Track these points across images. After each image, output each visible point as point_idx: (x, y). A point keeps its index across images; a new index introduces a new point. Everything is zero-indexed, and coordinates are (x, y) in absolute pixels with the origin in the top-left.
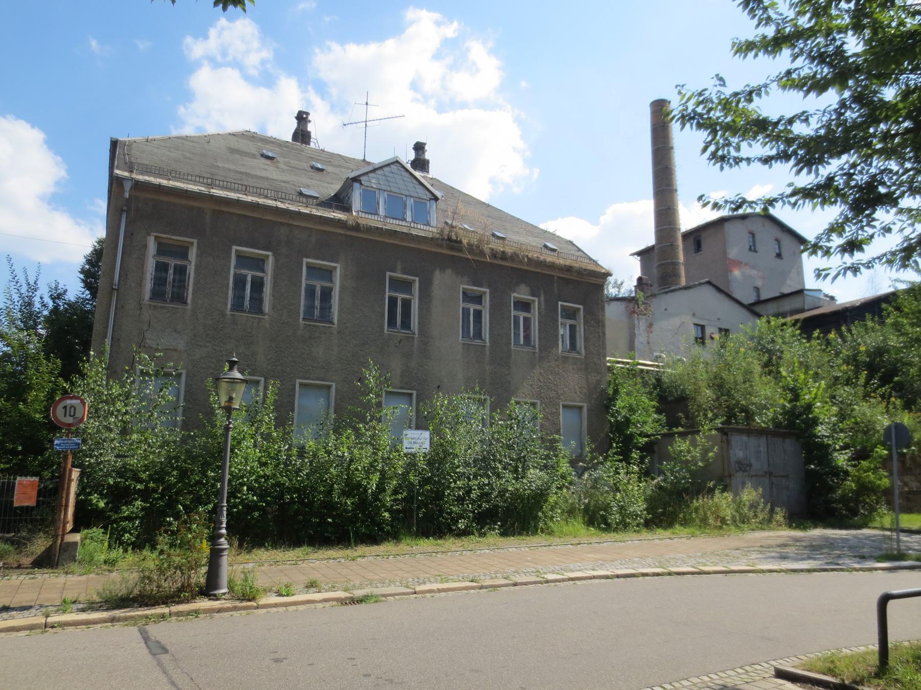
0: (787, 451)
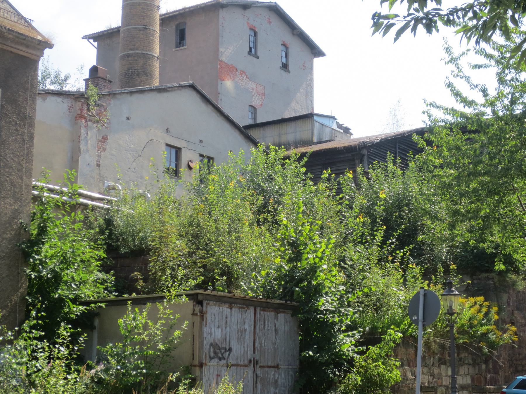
0: (280, 329)
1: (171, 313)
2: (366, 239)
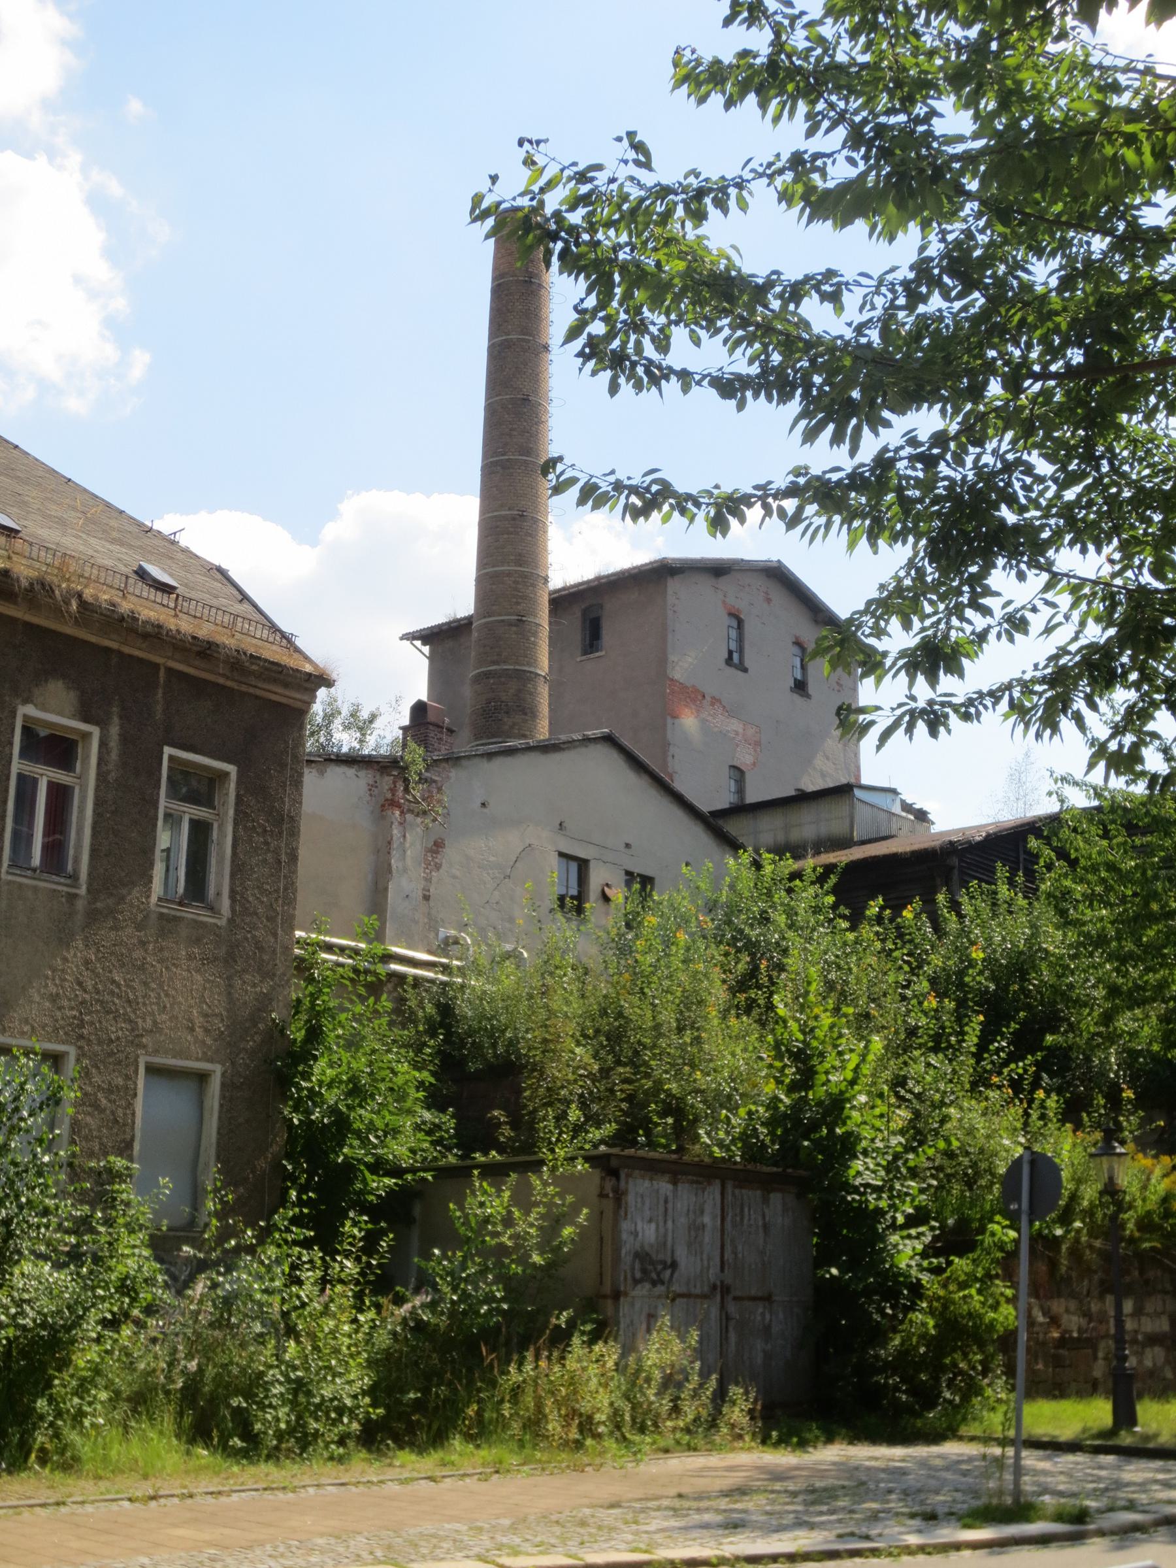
1: (557, 1194)
2: (948, 1041)
